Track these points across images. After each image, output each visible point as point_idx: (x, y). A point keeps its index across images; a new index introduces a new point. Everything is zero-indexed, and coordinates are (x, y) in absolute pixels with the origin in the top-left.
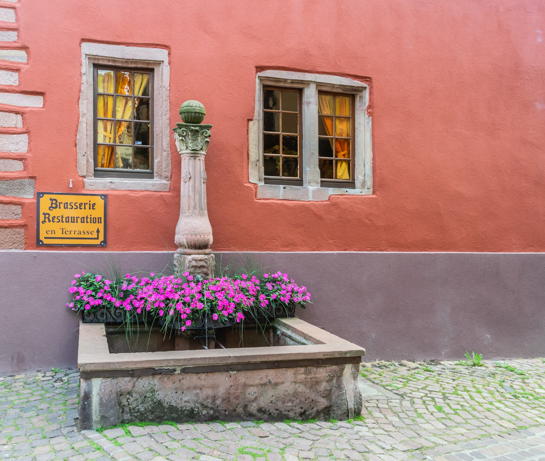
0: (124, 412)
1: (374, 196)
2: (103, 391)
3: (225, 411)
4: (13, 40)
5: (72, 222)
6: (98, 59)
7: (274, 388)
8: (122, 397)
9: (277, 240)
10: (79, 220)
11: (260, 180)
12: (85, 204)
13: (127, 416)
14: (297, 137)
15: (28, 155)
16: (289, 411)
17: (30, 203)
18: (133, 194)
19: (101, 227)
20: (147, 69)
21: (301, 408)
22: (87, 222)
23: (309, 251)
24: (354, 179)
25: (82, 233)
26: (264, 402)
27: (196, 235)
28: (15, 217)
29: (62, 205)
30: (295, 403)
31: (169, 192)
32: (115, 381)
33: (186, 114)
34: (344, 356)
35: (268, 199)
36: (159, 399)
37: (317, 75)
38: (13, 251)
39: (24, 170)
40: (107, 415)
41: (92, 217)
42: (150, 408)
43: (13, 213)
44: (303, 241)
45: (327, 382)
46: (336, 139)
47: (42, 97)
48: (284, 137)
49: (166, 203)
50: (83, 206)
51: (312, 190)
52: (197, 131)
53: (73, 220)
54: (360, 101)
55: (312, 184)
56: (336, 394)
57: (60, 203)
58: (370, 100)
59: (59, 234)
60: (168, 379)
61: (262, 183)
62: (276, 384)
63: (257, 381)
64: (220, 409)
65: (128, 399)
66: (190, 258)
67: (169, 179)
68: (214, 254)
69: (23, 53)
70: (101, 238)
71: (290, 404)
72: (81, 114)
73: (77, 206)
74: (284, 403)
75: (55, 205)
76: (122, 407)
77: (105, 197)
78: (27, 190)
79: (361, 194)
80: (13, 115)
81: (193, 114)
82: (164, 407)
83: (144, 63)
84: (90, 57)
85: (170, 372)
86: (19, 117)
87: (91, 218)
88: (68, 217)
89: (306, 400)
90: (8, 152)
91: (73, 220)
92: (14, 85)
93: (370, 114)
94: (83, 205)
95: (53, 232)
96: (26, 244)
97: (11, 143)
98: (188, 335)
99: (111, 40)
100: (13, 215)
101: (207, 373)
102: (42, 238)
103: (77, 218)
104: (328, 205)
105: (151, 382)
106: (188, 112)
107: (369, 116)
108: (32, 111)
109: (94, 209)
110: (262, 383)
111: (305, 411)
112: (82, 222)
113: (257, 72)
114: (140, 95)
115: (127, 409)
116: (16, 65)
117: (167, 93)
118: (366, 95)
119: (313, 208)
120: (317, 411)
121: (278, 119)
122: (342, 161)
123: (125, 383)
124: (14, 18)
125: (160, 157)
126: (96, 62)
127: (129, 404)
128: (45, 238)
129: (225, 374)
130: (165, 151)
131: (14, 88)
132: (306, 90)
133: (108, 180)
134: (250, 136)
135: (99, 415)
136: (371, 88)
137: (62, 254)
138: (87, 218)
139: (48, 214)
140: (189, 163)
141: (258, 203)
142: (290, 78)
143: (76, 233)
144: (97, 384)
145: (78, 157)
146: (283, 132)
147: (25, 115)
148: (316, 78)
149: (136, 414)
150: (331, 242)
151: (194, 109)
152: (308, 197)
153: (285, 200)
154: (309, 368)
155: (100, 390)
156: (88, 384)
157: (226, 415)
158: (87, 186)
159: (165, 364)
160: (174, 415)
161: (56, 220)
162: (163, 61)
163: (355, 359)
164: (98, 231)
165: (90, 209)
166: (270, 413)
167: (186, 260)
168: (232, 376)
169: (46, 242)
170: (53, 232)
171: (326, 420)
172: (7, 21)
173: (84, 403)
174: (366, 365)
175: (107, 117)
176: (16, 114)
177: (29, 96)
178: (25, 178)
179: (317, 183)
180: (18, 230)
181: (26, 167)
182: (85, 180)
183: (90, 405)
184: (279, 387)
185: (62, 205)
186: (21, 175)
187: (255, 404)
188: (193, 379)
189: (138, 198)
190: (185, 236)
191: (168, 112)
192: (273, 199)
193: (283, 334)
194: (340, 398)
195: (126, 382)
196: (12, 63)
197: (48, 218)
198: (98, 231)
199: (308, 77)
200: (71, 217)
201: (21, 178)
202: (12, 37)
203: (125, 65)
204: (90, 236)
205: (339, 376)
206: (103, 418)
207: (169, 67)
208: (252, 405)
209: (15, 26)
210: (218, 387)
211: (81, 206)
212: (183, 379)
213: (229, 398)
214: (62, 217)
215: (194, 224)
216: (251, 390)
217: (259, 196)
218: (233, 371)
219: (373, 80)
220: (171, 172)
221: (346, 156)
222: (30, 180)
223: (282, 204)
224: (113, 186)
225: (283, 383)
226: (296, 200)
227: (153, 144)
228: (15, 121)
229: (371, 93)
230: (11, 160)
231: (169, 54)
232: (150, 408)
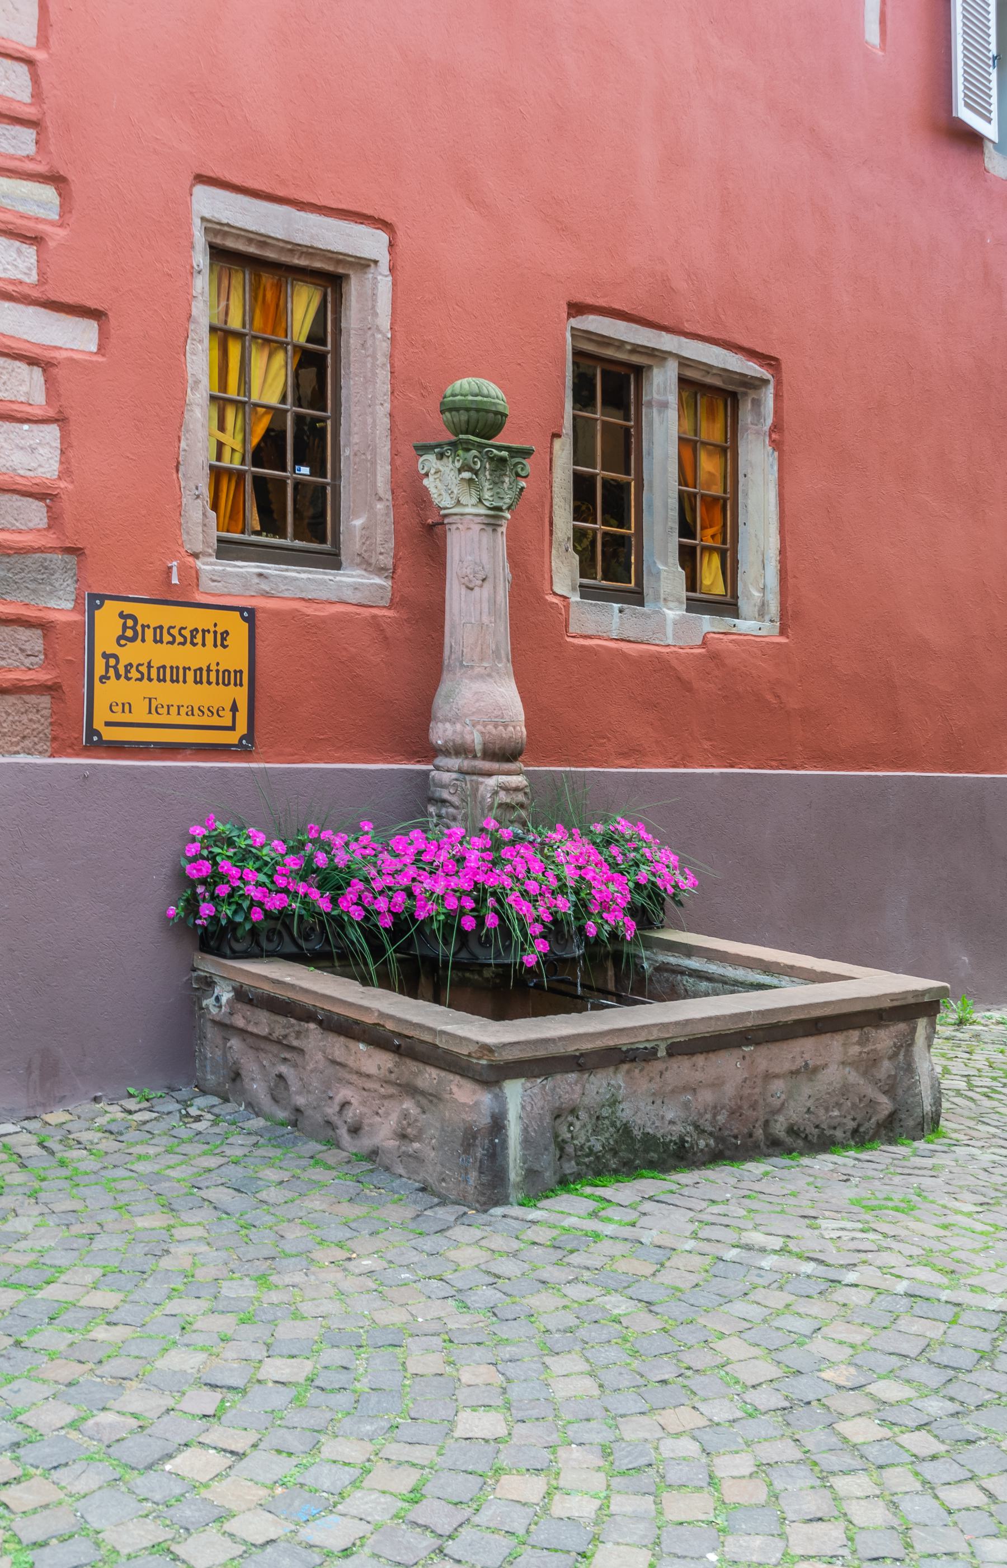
0: (565, 1157)
1: (783, 640)
2: (529, 1109)
3: (736, 1137)
4: (25, 154)
5: (172, 681)
6: (226, 234)
7: (811, 1080)
8: (559, 1121)
9: (609, 740)
10: (190, 675)
11: (574, 589)
12: (203, 631)
13: (570, 1167)
14: (629, 484)
15: (62, 484)
16: (835, 1128)
17: (68, 624)
18: (310, 610)
19: (241, 695)
20: (331, 279)
21: (854, 1119)
22: (209, 683)
23: (666, 766)
24: (735, 596)
25: (196, 711)
26: (795, 1113)
27: (506, 726)
28: (27, 662)
29: (149, 634)
30: (845, 1108)
31: (389, 608)
32: (549, 1084)
33: (473, 413)
34: (920, 1000)
35: (590, 637)
36: (624, 1121)
37: (683, 340)
38: (22, 759)
39: (50, 527)
40: (537, 1167)
41: (221, 669)
42: (612, 1142)
43: (22, 650)
44: (657, 742)
45: (890, 1058)
46: (703, 496)
47: (94, 325)
48: (605, 482)
49: (386, 638)
50: (199, 639)
51: (666, 620)
52: (503, 460)
53: (174, 675)
54: (752, 409)
55: (671, 605)
56: (906, 1083)
57: (143, 626)
58: (776, 412)
59: (140, 714)
60: (641, 1071)
61: (575, 598)
62: (816, 1070)
63: (787, 1066)
64: (726, 1133)
65: (571, 1124)
66: (492, 782)
67: (389, 573)
68: (527, 774)
69: (48, 193)
70: (242, 728)
71: (836, 1113)
72: (190, 381)
73: (185, 638)
74: (827, 1109)
75: (131, 631)
76: (562, 1146)
77: (249, 615)
78: (57, 584)
79: (760, 633)
80: (22, 367)
81: (491, 415)
82: (633, 1139)
83: (331, 259)
84: (209, 225)
85: (649, 1055)
86: (37, 372)
87: (217, 671)
88: (164, 667)
89: (860, 1100)
90: (12, 474)
91: (174, 675)
92: (28, 281)
93: (777, 445)
94: (200, 634)
95: (127, 707)
96: (54, 739)
97: (17, 446)
98: (487, 980)
99: (264, 188)
100: (22, 657)
101: (708, 1052)
102: (98, 724)
103: (184, 669)
104: (704, 656)
105: (613, 1082)
106: (478, 410)
107: (774, 449)
108: (71, 360)
110: (794, 1068)
111: (859, 1125)
112: (196, 682)
113: (570, 315)
114: (301, 339)
115: (570, 1149)
116: (31, 224)
117: (385, 346)
118: (768, 396)
119: (674, 663)
120: (878, 1123)
122: (711, 549)
123: (567, 1086)
124: (29, 90)
125: (365, 516)
126: (218, 241)
127: (572, 1138)
128: (108, 724)
129: (737, 1053)
130: (380, 499)
131: (26, 290)
132: (655, 371)
133: (251, 568)
134: (554, 475)
135: (521, 1168)
136: (779, 384)
137: (152, 770)
138: (209, 670)
139: (115, 657)
140: (480, 541)
141: (573, 645)
142: (632, 341)
143: (183, 711)
144: (515, 1093)
145: (184, 501)
146: (603, 469)
147: (55, 371)
148: (680, 346)
149: (587, 1160)
150: (707, 745)
151: (495, 404)
152: (665, 634)
153: (622, 640)
154: (865, 1029)
155: (523, 1107)
156: (496, 1097)
157: (737, 1146)
158: (205, 583)
159: (643, 1036)
160: (654, 1156)
161: (134, 674)
162: (376, 262)
163: (922, 1008)
164: (234, 708)
165: (215, 646)
166: (807, 1136)
167: (482, 788)
168: (747, 1058)
169: (110, 734)
170: (127, 707)
171: (891, 1141)
172: (10, 94)
173: (492, 1141)
174: (947, 1016)
175: (225, 392)
176: (29, 364)
177: (62, 316)
178: (53, 550)
179: (681, 602)
180: (32, 699)
181: (54, 520)
182: (199, 564)
183: (504, 1142)
184: (819, 1076)
185: (149, 634)
186: (41, 542)
187: (781, 1118)
188: (682, 1070)
189: (323, 620)
190: (480, 727)
191: (388, 398)
192: (600, 638)
193: (662, 968)
194: (911, 1092)
195: (570, 1084)
196: (22, 216)
197: (115, 668)
198: (234, 708)
199: (667, 342)
200: (172, 668)
201: (41, 550)
202: (21, 142)
203: (285, 259)
204: (215, 721)
205: (906, 1044)
206: (531, 1174)
207: (390, 278)
208: (776, 1121)
209: (31, 112)
210: (723, 1083)
211: (193, 637)
212: (667, 1069)
213: (740, 1107)
214: (149, 666)
215: (483, 697)
216: (778, 1086)
217: (573, 629)
218: (747, 1045)
219: (783, 366)
220: (395, 556)
221: (719, 538)
222: (67, 557)
223: (617, 650)
224: (265, 586)
225: (825, 1066)
226: (641, 643)
227: (337, 475)
228: (26, 386)
229: (778, 397)
230: (16, 497)
231: (391, 245)
232: (612, 1142)
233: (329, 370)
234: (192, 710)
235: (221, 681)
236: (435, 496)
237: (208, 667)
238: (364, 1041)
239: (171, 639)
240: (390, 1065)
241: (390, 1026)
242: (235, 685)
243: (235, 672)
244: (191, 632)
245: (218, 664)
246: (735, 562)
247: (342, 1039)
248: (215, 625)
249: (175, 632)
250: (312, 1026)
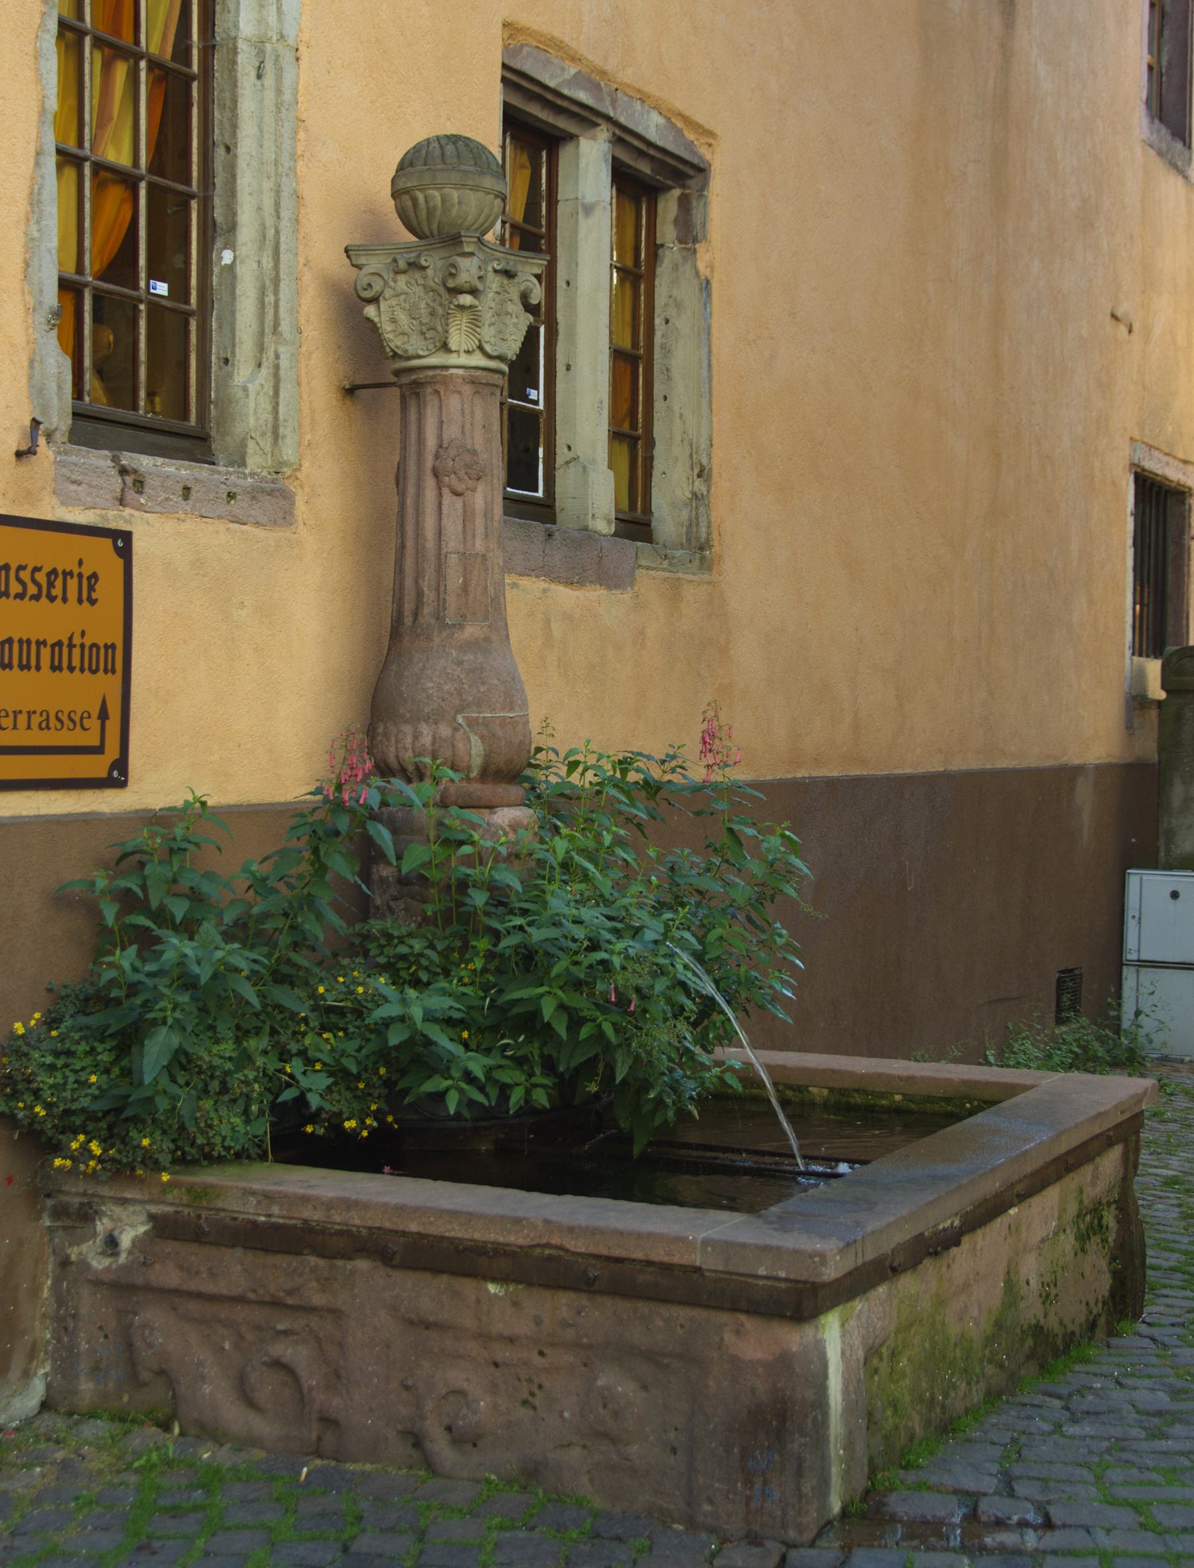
22: (71, 669)
25: (53, 722)
87: (82, 646)
103: (38, 643)
109: (93, 602)
138: (71, 646)
165: (80, 601)
198: (103, 715)
233: (195, 111)
234: (48, 719)
235: (86, 666)
236: (391, 336)
237: (71, 639)
238: (494, 1280)
239: (19, 589)
240: (564, 1312)
241: (578, 1245)
242: (106, 671)
243: (106, 647)
244: (49, 575)
245: (83, 634)
246: (649, 461)
247: (444, 1279)
248: (81, 563)
249: (25, 575)
250: (362, 1264)
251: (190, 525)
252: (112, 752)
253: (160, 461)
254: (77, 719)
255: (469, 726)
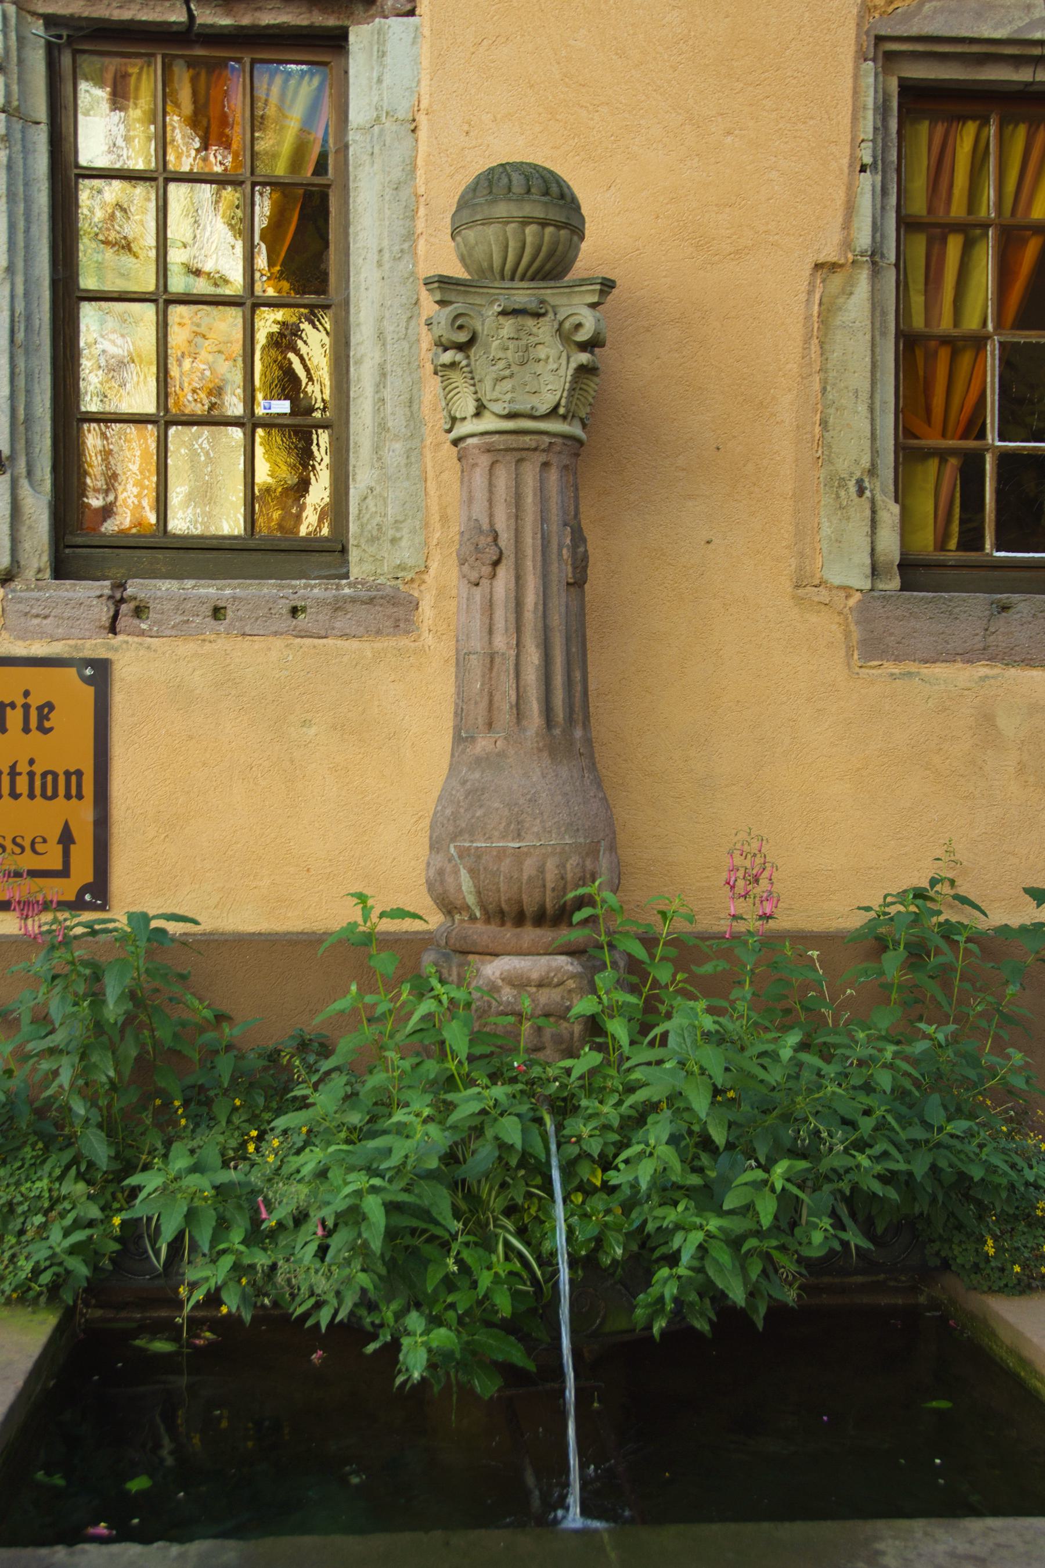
19: (82, 815)
41: (38, 769)
87: (31, 775)
121: (991, 499)
138: (13, 773)
164: (66, 838)
165: (26, 730)
198: (66, 838)
206: (317, 293)
237: (13, 767)
242: (68, 796)
245: (32, 762)
251: (222, 644)
252: (83, 871)
253: (189, 583)
254: (27, 844)
255: (461, 857)
